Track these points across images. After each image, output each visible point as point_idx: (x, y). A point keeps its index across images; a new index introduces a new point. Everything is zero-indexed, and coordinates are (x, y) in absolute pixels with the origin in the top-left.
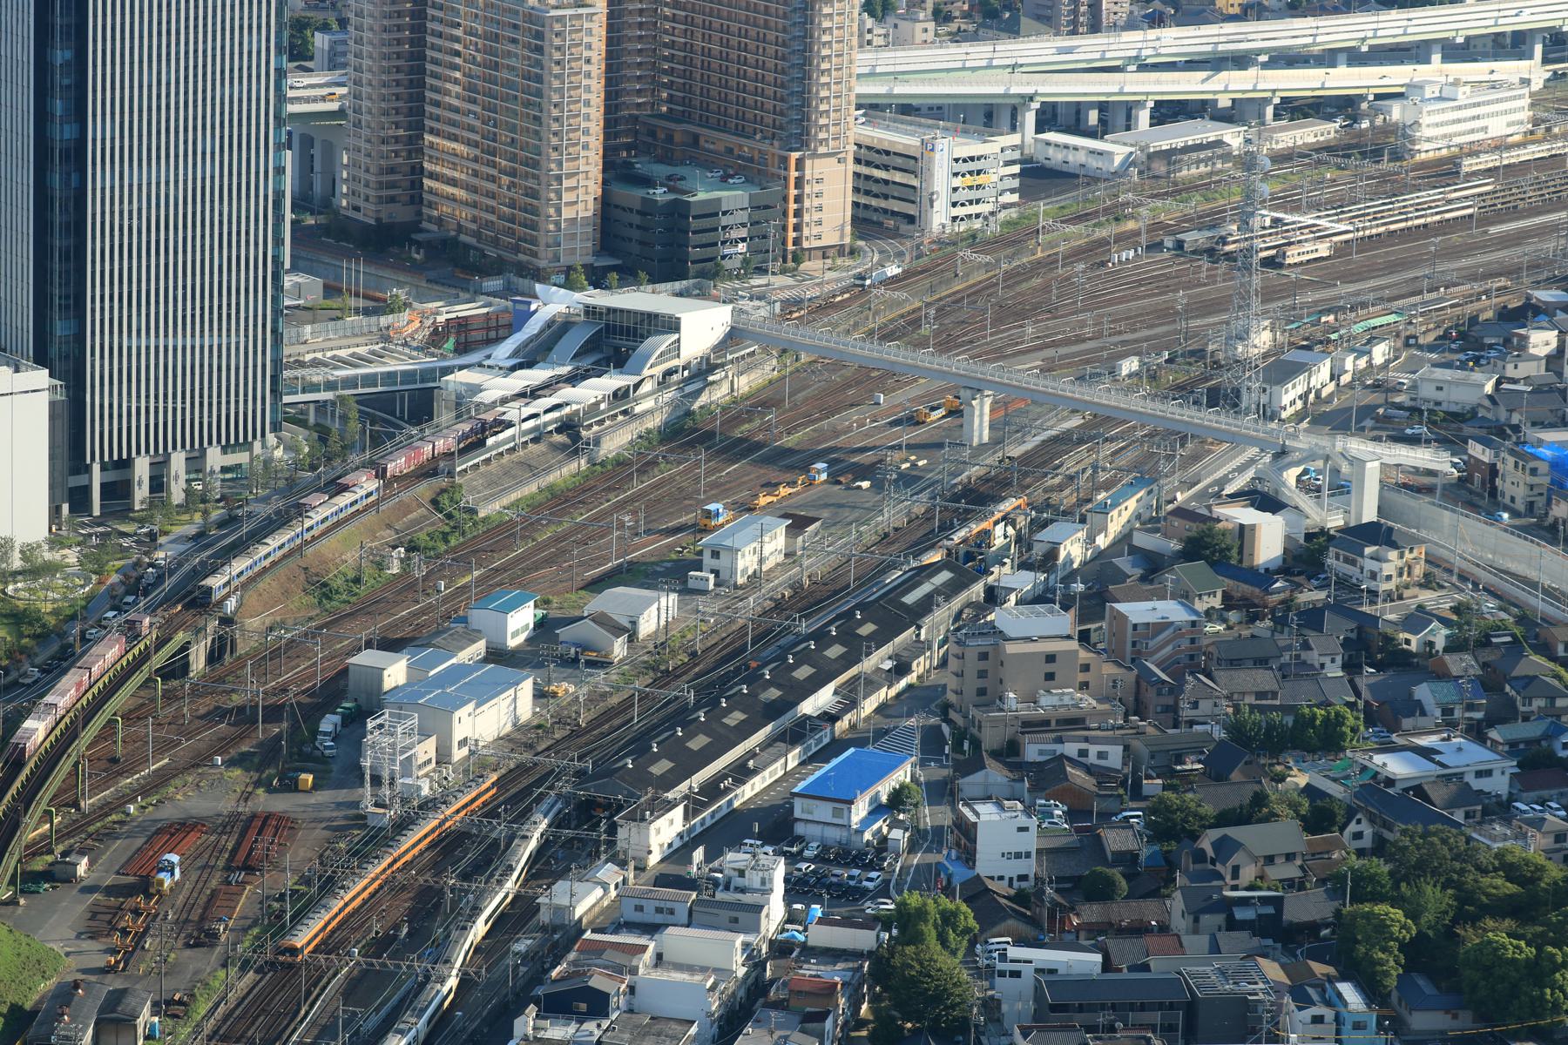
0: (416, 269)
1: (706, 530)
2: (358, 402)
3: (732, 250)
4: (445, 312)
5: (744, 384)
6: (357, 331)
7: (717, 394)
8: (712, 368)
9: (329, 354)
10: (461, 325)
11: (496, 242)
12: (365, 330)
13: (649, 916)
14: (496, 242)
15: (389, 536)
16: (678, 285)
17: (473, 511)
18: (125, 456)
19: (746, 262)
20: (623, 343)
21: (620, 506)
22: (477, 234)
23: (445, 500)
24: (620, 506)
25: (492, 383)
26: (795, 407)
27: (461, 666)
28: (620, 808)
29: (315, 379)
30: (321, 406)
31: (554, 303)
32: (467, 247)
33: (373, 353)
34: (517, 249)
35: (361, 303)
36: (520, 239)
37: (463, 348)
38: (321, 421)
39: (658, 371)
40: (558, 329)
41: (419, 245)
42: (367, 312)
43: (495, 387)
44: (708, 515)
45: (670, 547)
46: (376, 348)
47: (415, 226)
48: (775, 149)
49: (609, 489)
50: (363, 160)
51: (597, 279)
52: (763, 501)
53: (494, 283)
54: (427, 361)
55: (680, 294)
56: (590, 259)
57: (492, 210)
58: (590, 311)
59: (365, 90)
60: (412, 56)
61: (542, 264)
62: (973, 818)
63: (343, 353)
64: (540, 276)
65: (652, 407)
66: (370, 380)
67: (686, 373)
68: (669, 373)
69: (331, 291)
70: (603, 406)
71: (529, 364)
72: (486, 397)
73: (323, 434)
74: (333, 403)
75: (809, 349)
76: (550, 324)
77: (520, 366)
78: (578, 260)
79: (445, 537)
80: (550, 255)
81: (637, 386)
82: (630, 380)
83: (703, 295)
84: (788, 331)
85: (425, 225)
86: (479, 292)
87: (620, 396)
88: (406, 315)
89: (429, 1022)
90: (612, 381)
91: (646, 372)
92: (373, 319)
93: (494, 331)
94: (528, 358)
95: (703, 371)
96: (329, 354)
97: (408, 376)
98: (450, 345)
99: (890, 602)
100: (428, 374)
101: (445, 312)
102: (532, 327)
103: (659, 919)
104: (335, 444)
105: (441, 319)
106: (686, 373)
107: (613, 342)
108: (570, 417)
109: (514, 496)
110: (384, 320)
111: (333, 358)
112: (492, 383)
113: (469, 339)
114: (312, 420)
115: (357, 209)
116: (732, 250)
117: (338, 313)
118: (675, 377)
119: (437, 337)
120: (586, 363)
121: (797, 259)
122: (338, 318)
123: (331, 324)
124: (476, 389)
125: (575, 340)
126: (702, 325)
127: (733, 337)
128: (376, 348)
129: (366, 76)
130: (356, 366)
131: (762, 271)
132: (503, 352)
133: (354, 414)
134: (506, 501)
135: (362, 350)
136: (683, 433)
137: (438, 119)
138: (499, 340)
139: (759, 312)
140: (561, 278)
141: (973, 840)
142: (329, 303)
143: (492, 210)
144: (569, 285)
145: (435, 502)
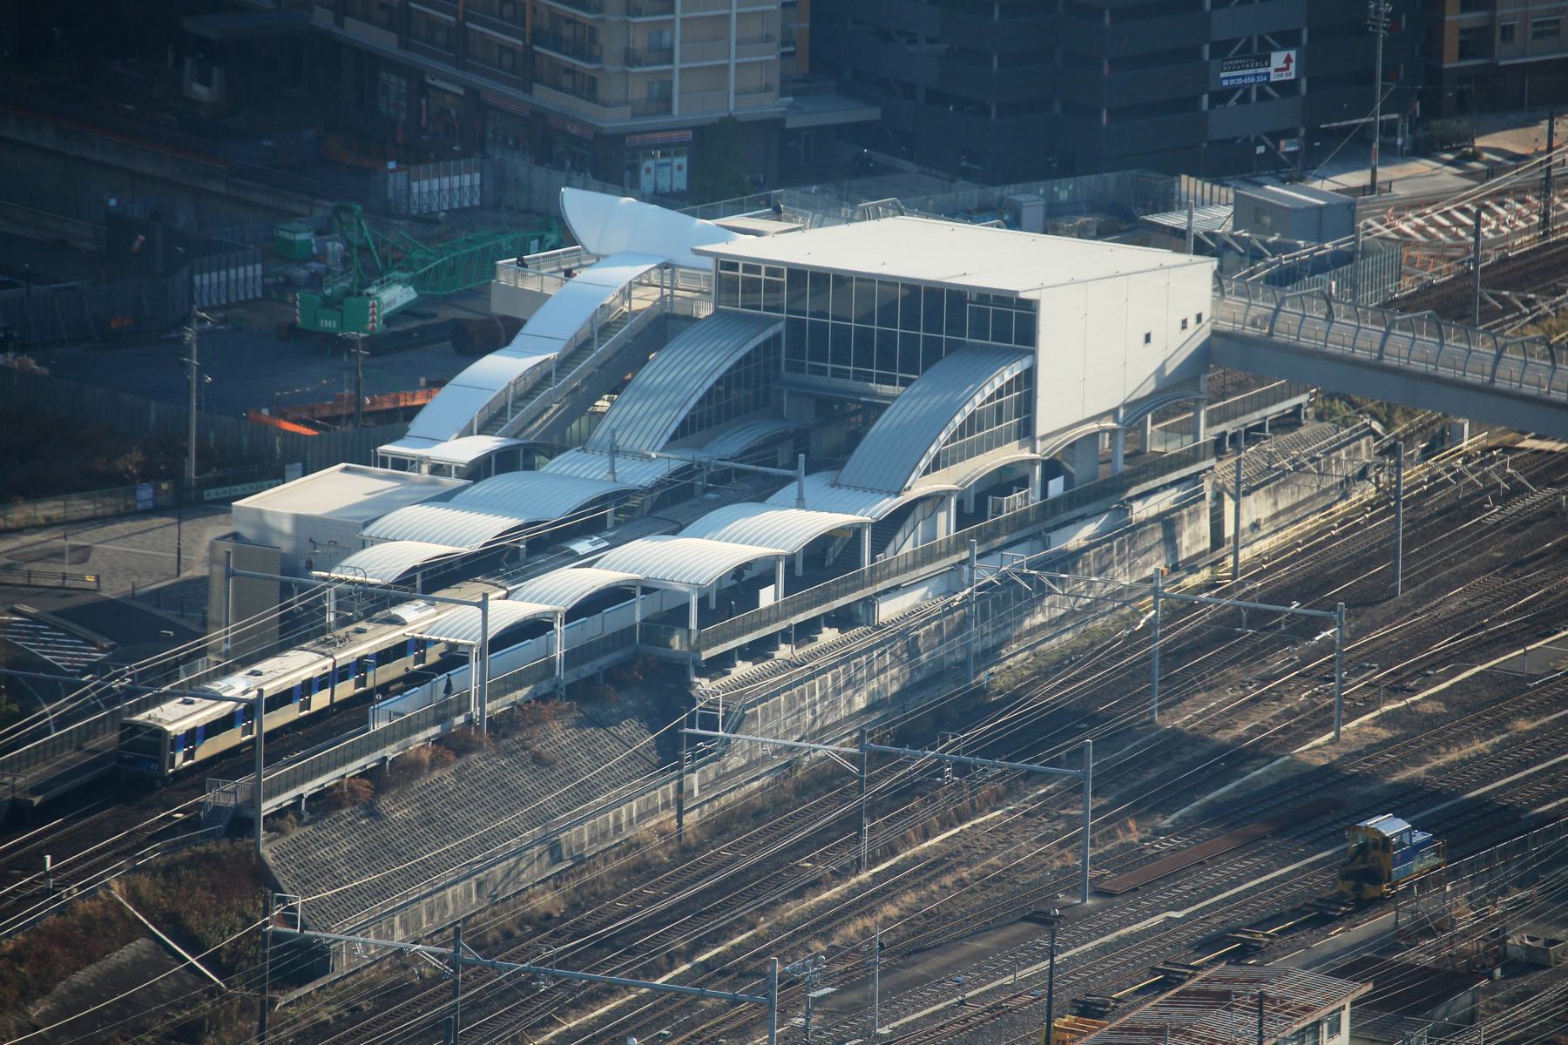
3: (1245, 75)
18: (461, 91)
27: (119, 970)
32: (369, 61)
34: (527, 71)
36: (537, 37)
40: (620, 351)
56: (771, 105)
58: (735, 280)
67: (1056, 487)
70: (767, 597)
80: (639, 91)
81: (887, 529)
83: (1123, 222)
87: (823, 561)
90: (785, 526)
95: (1096, 479)
106: (1056, 487)
116: (1245, 75)
118: (1015, 502)
120: (726, 447)
125: (684, 374)
127: (1212, 371)
140: (676, 172)
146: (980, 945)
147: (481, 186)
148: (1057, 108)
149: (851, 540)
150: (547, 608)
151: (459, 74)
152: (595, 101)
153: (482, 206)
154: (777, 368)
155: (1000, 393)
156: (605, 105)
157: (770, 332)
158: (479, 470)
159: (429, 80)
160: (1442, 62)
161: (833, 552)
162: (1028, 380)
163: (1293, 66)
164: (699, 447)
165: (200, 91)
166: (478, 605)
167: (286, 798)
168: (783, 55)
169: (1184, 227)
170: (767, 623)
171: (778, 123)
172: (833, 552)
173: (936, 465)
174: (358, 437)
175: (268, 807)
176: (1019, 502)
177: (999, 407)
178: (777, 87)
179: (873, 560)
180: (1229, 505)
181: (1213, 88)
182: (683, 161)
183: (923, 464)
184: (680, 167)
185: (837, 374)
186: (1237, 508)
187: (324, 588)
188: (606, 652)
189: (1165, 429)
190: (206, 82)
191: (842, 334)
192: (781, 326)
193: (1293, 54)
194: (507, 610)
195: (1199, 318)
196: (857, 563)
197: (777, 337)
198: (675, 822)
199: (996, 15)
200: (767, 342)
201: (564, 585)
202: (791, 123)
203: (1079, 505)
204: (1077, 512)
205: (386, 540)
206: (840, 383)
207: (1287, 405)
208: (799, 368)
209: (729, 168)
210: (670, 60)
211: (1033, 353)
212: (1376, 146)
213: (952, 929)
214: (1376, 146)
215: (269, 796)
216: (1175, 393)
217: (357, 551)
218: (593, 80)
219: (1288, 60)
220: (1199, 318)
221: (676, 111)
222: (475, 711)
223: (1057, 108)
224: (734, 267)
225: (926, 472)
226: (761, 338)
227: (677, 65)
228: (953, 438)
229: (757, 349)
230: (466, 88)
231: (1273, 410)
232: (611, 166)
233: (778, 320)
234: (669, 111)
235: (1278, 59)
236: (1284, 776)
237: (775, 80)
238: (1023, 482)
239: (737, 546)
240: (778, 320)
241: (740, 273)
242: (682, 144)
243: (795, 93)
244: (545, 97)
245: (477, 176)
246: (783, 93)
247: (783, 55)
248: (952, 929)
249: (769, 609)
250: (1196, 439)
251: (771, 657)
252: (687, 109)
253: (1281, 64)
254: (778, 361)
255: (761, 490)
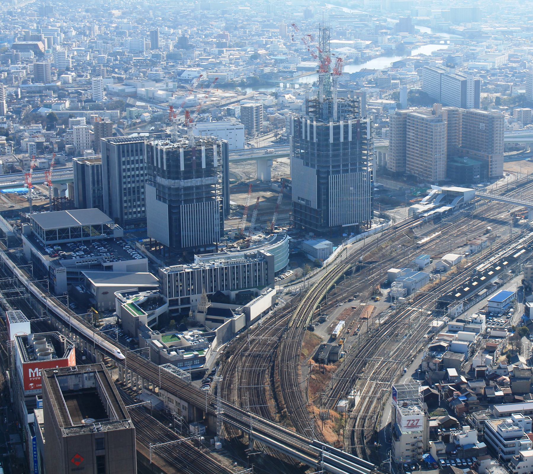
11: (423, 176)
13: (454, 329)
14: (423, 176)
22: (418, 174)
28: (449, 304)
31: (435, 190)
32: (416, 177)
40: (435, 196)
41: (405, 176)
47: (404, 172)
48: (486, 154)
50: (393, 158)
56: (444, 179)
57: (421, 168)
58: (444, 192)
59: (393, 141)
60: (404, 124)
62: (529, 306)
77: (428, 204)
85: (407, 172)
89: (441, 50)
94: (430, 201)
99: (354, 452)
103: (457, 329)
115: (391, 168)
120: (442, 203)
124: (418, 209)
125: (440, 198)
129: (393, 145)
137: (409, 154)
141: (529, 311)
143: (421, 168)
158: (426, 204)
169: (93, 386)
174: (418, 202)
194: (429, 214)
198: (115, 420)
201: (432, 212)
209: (441, 184)
232: (433, 184)
236: (232, 395)
244: (428, 179)
252: (438, 180)
253: (478, 176)
255: (445, 205)
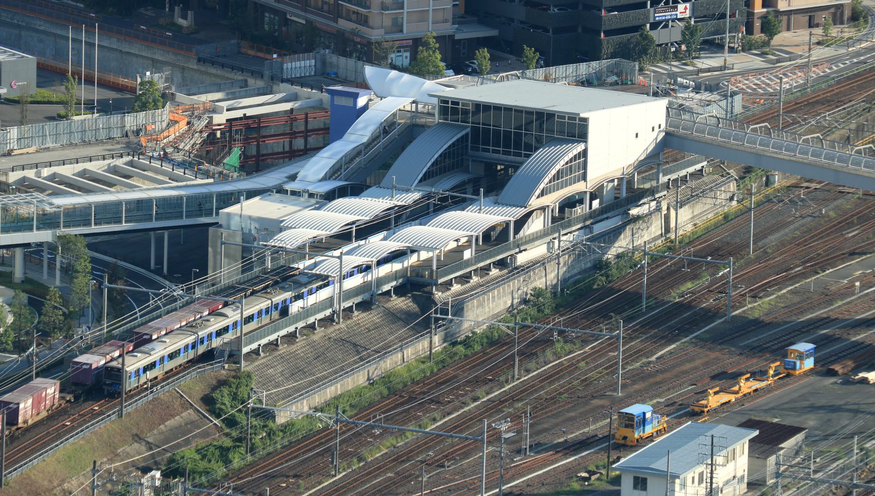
0: (182, 41)
1: (625, 446)
2: (90, 246)
4: (226, 109)
5: (686, 220)
6: (89, 136)
7: (644, 236)
8: (636, 196)
9: (46, 172)
10: (250, 129)
12: (103, 135)
15: (138, 453)
16: (584, 69)
17: (267, 415)
18: (304, 22)
19: (689, 32)
20: (499, 157)
21: (494, 408)
23: (224, 398)
24: (494, 408)
25: (294, 216)
26: (764, 255)
29: (24, 211)
30: (33, 252)
31: (392, 95)
33: (114, 170)
35: (97, 94)
37: (253, 164)
38: (32, 275)
39: (553, 199)
40: (399, 136)
42: (105, 108)
43: (304, 224)
44: (629, 421)
45: (570, 472)
46: (120, 162)
49: (478, 382)
51: (460, 61)
52: (714, 400)
53: (300, 65)
54: (198, 184)
55: (586, 83)
56: (448, 29)
58: (450, 109)
61: (375, 35)
63: (68, 171)
64: (372, 54)
65: (543, 255)
66: (109, 212)
67: (596, 204)
68: (570, 203)
69: (48, 74)
70: (467, 254)
71: (355, 190)
72: (291, 239)
73: (35, 296)
74: (52, 248)
75: (787, 166)
76: (387, 127)
78: (431, 30)
79: (224, 454)
80: (388, 22)
82: (510, 214)
83: (622, 83)
84: (756, 140)
86: (277, 78)
87: (495, 238)
88: (165, 114)
90: (480, 217)
91: (535, 202)
92: (115, 119)
93: (304, 137)
94: (352, 181)
95: (622, 200)
96: (46, 172)
97: (169, 207)
98: (233, 158)
100: (200, 204)
101: (226, 109)
102: (361, 132)
104: (54, 313)
105: (220, 119)
106: (596, 204)
107: (484, 156)
108: (417, 270)
109: (331, 391)
110: (131, 121)
111: (53, 177)
112: (294, 216)
113: (262, 150)
114: (18, 273)
117: (61, 110)
118: (579, 210)
119: (213, 146)
120: (443, 187)
121: (769, 28)
122: (60, 117)
123: (49, 126)
124: (274, 227)
125: (424, 153)
126: (621, 131)
127: (669, 148)
128: (120, 162)
130: (87, 191)
131: (714, 46)
132: (315, 169)
133: (84, 265)
134: (318, 399)
135: (97, 167)
136: (590, 296)
138: (308, 152)
139: (709, 110)
140: (404, 58)
142: (45, 93)
144: (417, 68)
145: (208, 401)
146: (572, 414)
147: (315, 65)
148: (580, 30)
149: (504, 229)
150: (403, 244)
151: (303, 14)
152: (368, 27)
153: (315, 75)
154: (467, 149)
155: (571, 160)
156: (372, 28)
157: (464, 132)
159: (288, 17)
160: (753, 8)
161: (494, 235)
162: (584, 153)
163: (688, 11)
164: (432, 185)
165: (182, 22)
166: (338, 257)
167: (254, 346)
168: (454, 5)
170: (466, 267)
171: (451, 37)
172: (494, 235)
173: (542, 194)
175: (245, 350)
176: (579, 211)
177: (571, 167)
178: (451, 20)
179: (514, 237)
180: (673, 213)
181: (652, 21)
182: (408, 54)
183: (538, 192)
184: (406, 57)
185: (494, 151)
186: (677, 214)
187: (264, 252)
188: (357, 295)
189: (643, 178)
190: (185, 17)
191: (497, 133)
192: (469, 130)
193: (688, 5)
195: (660, 126)
196: (507, 239)
197: (467, 134)
199: (167, 10)
200: (462, 137)
202: (457, 37)
203: (606, 213)
204: (605, 216)
205: (291, 228)
206: (496, 156)
207: (698, 167)
208: (477, 149)
210: (403, 8)
211: (586, 142)
212: (726, 48)
213: (559, 407)
214: (726, 48)
215: (246, 345)
216: (652, 162)
217: (277, 234)
218: (366, 17)
219: (686, 8)
220: (660, 126)
221: (405, 31)
222: (336, 306)
223: (580, 30)
224: (447, 102)
225: (538, 197)
226: (459, 135)
227: (406, 10)
228: (550, 182)
229: (458, 140)
230: (306, 21)
231: (691, 170)
233: (467, 127)
234: (401, 31)
235: (681, 7)
237: (450, 18)
238: (581, 202)
239: (492, 216)
240: (467, 127)
241: (450, 105)
242: (407, 46)
243: (459, 23)
245: (313, 61)
246: (453, 23)
247: (454, 5)
248: (559, 407)
249: (468, 260)
250: (658, 182)
251: (488, 274)
254: (467, 146)
